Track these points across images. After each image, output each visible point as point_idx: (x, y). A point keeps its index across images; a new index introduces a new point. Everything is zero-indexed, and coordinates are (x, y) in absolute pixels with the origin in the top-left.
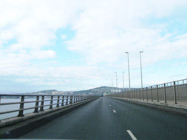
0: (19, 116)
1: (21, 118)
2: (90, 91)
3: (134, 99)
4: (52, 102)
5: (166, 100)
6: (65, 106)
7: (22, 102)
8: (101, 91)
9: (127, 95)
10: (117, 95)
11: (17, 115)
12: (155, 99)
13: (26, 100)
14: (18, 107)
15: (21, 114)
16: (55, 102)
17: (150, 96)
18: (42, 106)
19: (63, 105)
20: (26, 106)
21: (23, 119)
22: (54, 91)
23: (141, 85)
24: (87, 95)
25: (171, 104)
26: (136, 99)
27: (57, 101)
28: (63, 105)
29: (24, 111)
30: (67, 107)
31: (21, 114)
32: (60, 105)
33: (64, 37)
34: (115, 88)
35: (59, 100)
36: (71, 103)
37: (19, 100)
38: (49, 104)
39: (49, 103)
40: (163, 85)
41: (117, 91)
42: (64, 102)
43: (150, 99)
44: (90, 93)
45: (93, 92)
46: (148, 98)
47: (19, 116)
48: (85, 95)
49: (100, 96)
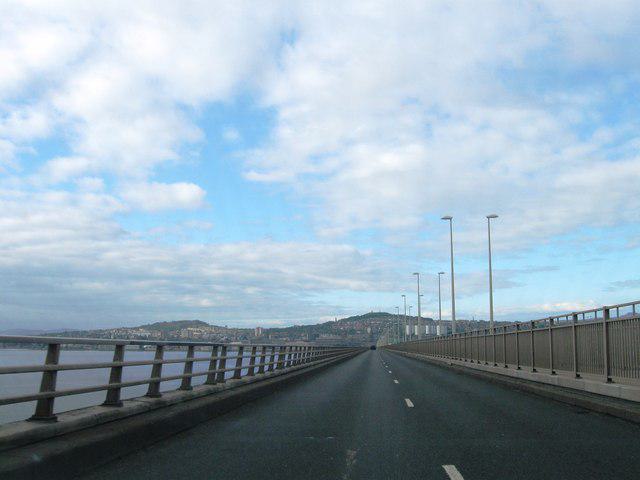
0: (181, 388)
1: (237, 380)
2: (328, 327)
3: (492, 363)
4: (189, 365)
5: (609, 374)
6: (268, 374)
7: (118, 363)
8: (369, 330)
9: (463, 346)
10: (429, 343)
11: (33, 413)
12: (565, 366)
13: (65, 357)
14: (104, 377)
15: (45, 406)
16: (201, 367)
17: (548, 355)
18: (155, 379)
19: (261, 370)
20: (127, 374)
21: (119, 413)
22: (198, 323)
23: (489, 312)
24: (313, 344)
25: (593, 383)
26: (483, 362)
27: (40, 375)
28: (251, 372)
29: (122, 389)
30: (252, 383)
31: (45, 406)
32: (244, 372)
33: (231, 135)
34: (414, 320)
35: (120, 368)
36: (280, 366)
37: (39, 357)
38: (234, 367)
39: (180, 369)
40: (601, 315)
41: (430, 330)
42: (243, 365)
43: (567, 369)
44: (324, 336)
45: (338, 333)
46: (555, 363)
47: (151, 397)
48: (306, 344)
49: (366, 349)
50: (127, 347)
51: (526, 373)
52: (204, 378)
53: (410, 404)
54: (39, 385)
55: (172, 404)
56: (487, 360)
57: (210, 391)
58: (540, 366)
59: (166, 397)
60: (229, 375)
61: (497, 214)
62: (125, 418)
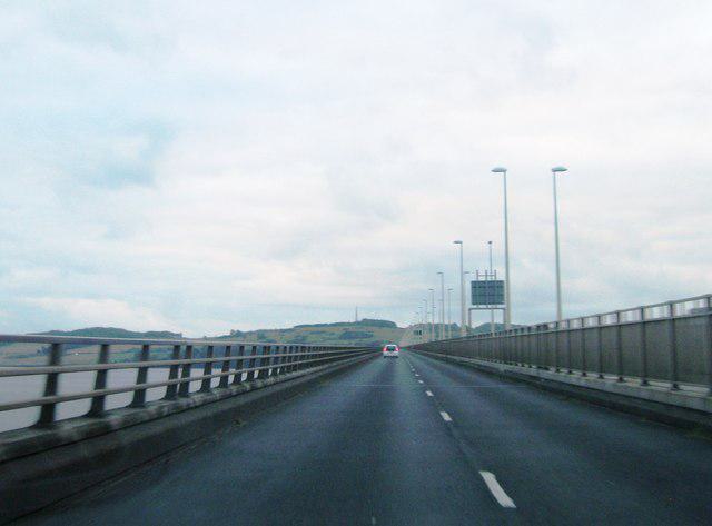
6: (234, 389)
12: (634, 374)
30: (205, 404)
47: (170, 399)
50: (65, 346)
51: (576, 377)
52: (162, 391)
53: (446, 417)
54: (135, 380)
55: (71, 443)
56: (571, 368)
57: (205, 401)
58: (685, 381)
59: (66, 430)
60: (195, 386)
61: (565, 167)
62: (142, 423)
